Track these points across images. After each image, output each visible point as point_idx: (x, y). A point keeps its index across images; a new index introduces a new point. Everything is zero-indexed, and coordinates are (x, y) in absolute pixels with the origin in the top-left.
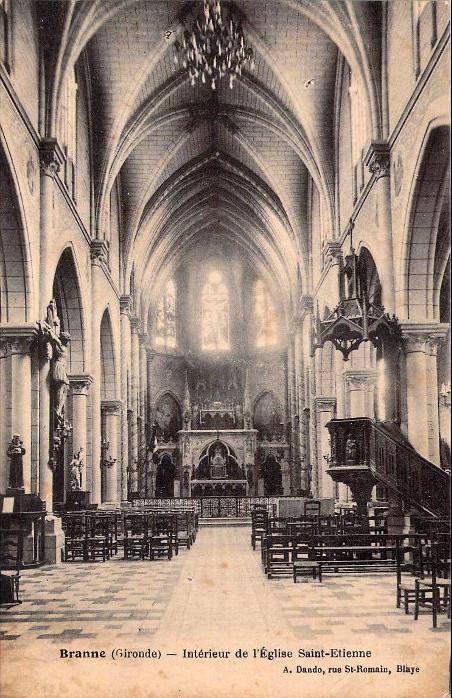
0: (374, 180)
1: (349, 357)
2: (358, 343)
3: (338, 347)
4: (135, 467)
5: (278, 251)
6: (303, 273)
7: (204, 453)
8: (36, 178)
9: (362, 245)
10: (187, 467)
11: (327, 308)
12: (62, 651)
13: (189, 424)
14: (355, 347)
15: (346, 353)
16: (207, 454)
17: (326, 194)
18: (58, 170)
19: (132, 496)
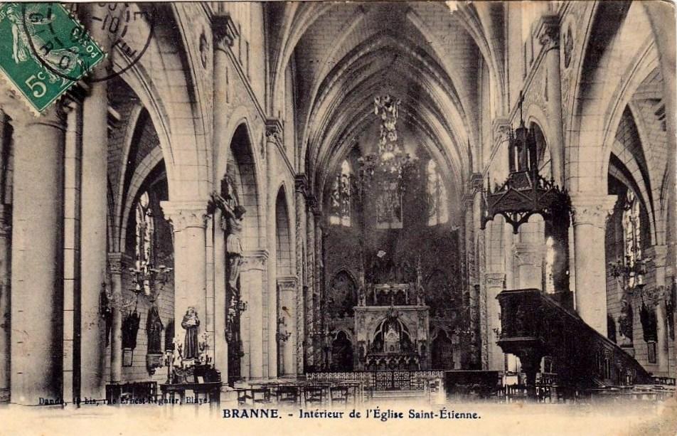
0: (543, 52)
1: (519, 230)
2: (527, 216)
3: (508, 220)
4: (310, 341)
5: (449, 130)
6: (473, 152)
7: (378, 329)
8: (209, 53)
9: (531, 120)
10: (363, 342)
11: (497, 184)
12: (225, 411)
13: (364, 301)
14: (525, 220)
15: (516, 226)
16: (381, 330)
17: (496, 70)
18: (232, 44)
19: (308, 369)
